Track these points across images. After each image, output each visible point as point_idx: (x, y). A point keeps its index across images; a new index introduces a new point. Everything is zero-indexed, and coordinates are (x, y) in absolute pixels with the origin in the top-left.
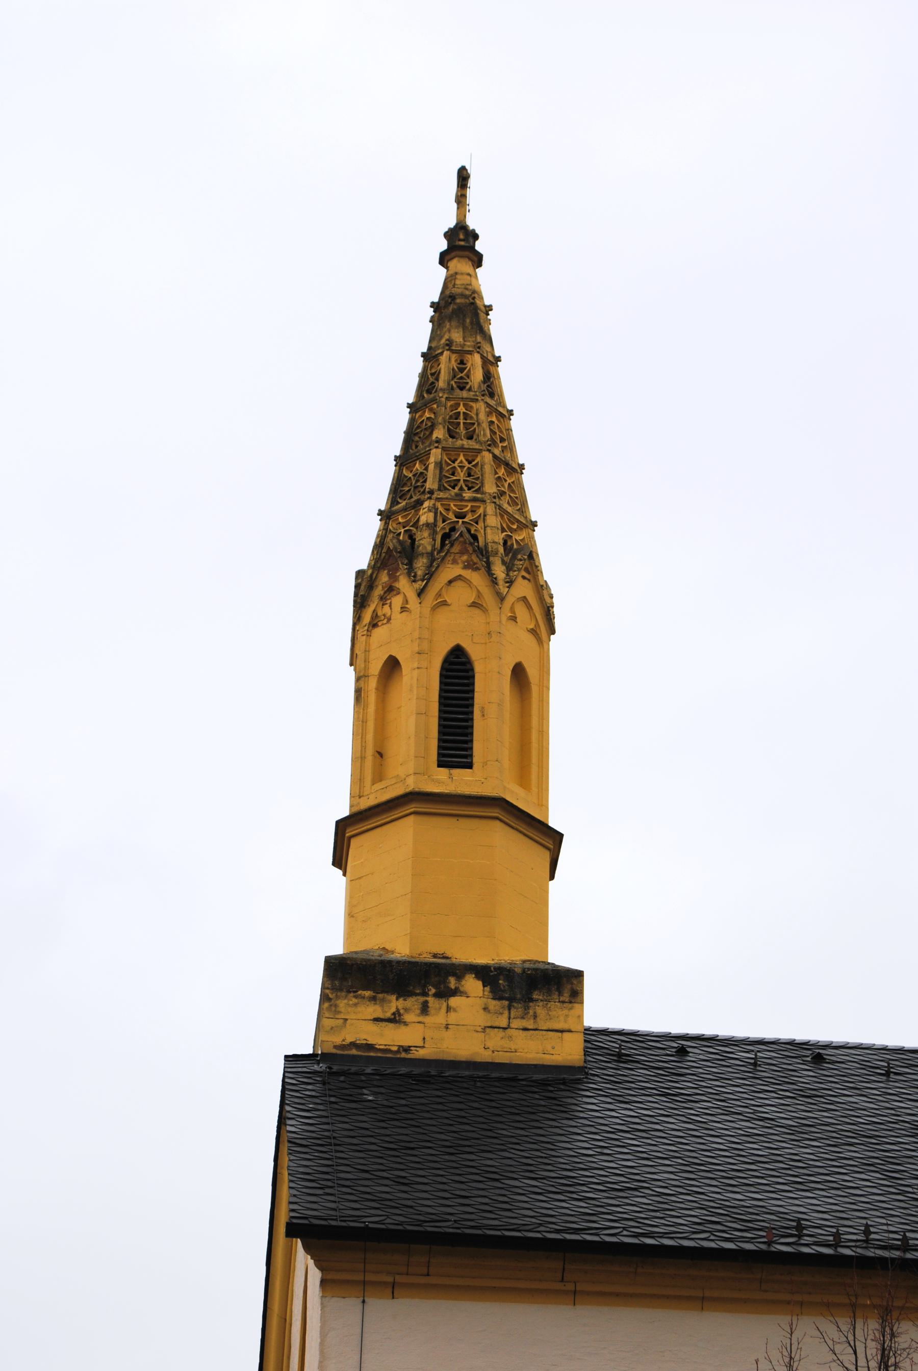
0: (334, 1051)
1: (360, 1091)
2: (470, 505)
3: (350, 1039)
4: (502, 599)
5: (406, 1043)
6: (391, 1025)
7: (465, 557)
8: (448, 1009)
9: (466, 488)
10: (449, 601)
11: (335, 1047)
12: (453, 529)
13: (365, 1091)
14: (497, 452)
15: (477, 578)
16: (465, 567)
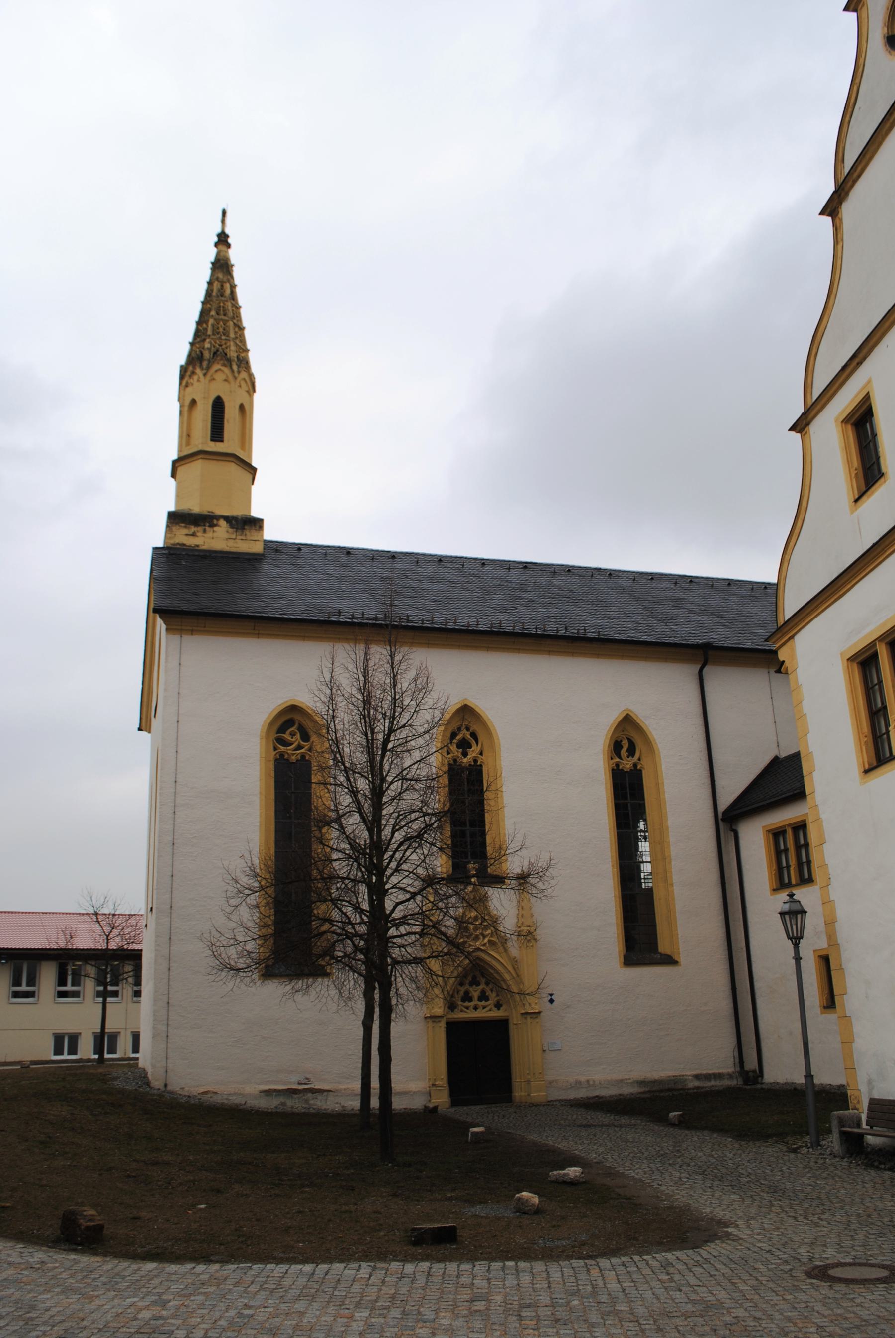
8: (214, 532)
14: (235, 321)
15: (227, 370)
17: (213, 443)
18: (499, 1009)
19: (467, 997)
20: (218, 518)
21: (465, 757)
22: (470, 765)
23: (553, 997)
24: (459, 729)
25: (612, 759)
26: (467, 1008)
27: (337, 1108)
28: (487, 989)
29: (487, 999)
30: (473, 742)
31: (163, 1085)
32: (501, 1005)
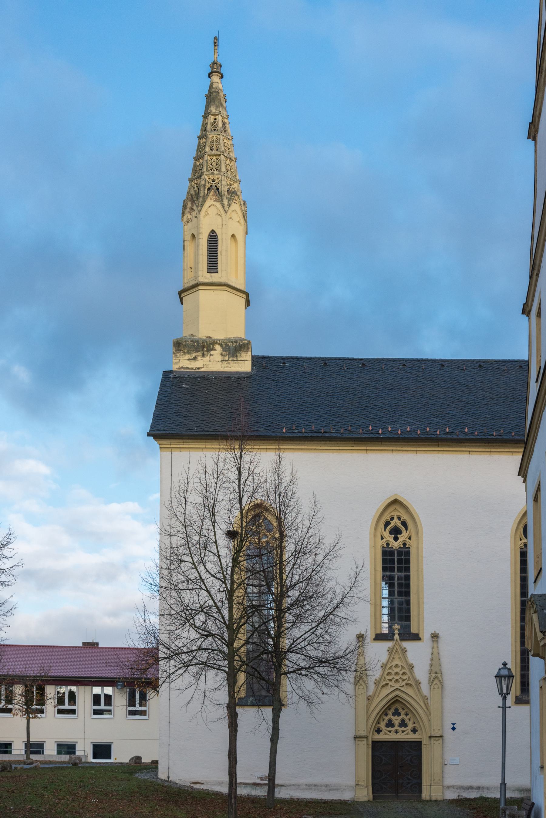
0: (177, 370)
1: (182, 384)
2: (216, 176)
3: (181, 366)
4: (226, 212)
5: (198, 367)
6: (193, 361)
7: (214, 197)
8: (211, 355)
9: (215, 170)
10: (209, 214)
11: (177, 369)
12: (211, 186)
13: (184, 384)
14: (226, 155)
15: (218, 205)
16: (214, 201)
17: (209, 274)
18: (415, 733)
19: (390, 724)
20: (214, 342)
21: (396, 541)
22: (400, 547)
23: (455, 726)
24: (392, 519)
25: (521, 540)
26: (390, 732)
27: (287, 796)
28: (406, 718)
29: (406, 726)
30: (403, 528)
31: (167, 777)
32: (417, 731)
